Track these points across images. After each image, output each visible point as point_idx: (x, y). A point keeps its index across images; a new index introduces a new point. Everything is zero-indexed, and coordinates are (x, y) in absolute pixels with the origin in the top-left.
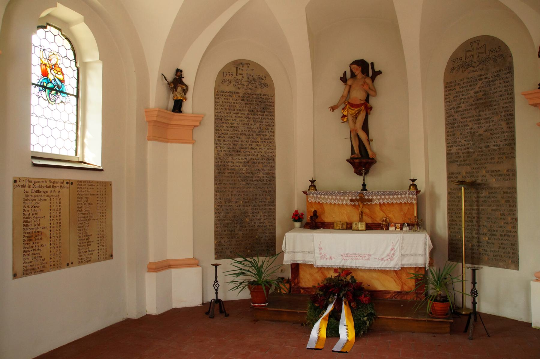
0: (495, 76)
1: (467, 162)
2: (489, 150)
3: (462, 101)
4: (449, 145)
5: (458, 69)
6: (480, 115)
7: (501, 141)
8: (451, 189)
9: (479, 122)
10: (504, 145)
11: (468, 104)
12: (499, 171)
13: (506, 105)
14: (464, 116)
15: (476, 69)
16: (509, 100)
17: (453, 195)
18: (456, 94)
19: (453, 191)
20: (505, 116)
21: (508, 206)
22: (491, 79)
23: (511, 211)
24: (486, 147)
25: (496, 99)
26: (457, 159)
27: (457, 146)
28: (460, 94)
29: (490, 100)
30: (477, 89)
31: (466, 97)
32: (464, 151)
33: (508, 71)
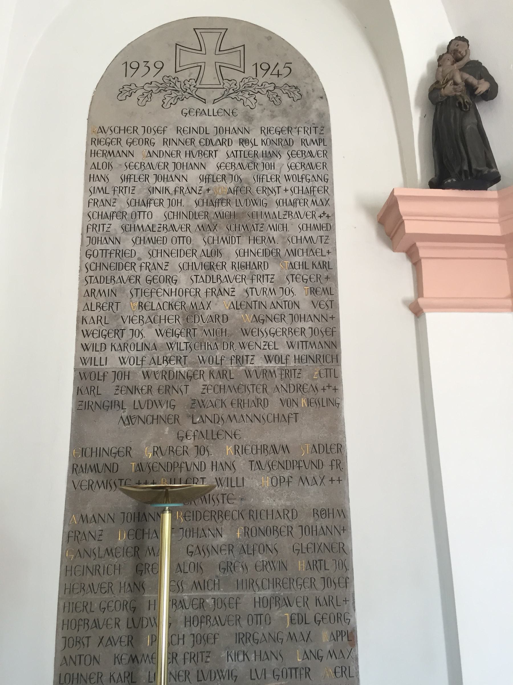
0: (272, 141)
1: (162, 411)
2: (248, 373)
3: (156, 196)
4: (89, 340)
5: (148, 95)
6: (218, 252)
7: (291, 345)
8: (84, 519)
9: (214, 273)
10: (300, 359)
11: (175, 209)
12: (285, 449)
13: (308, 234)
14: (159, 247)
15: (210, 106)
16: (319, 221)
17: (93, 544)
18: (135, 172)
19: (91, 526)
20: (304, 265)
21: (319, 584)
22: (261, 148)
23: (329, 601)
24: (239, 360)
25: (276, 209)
26: (120, 397)
27: (123, 347)
28: (151, 172)
29: (256, 209)
30: (211, 168)
31: (172, 185)
32: (153, 368)
33: (314, 136)
